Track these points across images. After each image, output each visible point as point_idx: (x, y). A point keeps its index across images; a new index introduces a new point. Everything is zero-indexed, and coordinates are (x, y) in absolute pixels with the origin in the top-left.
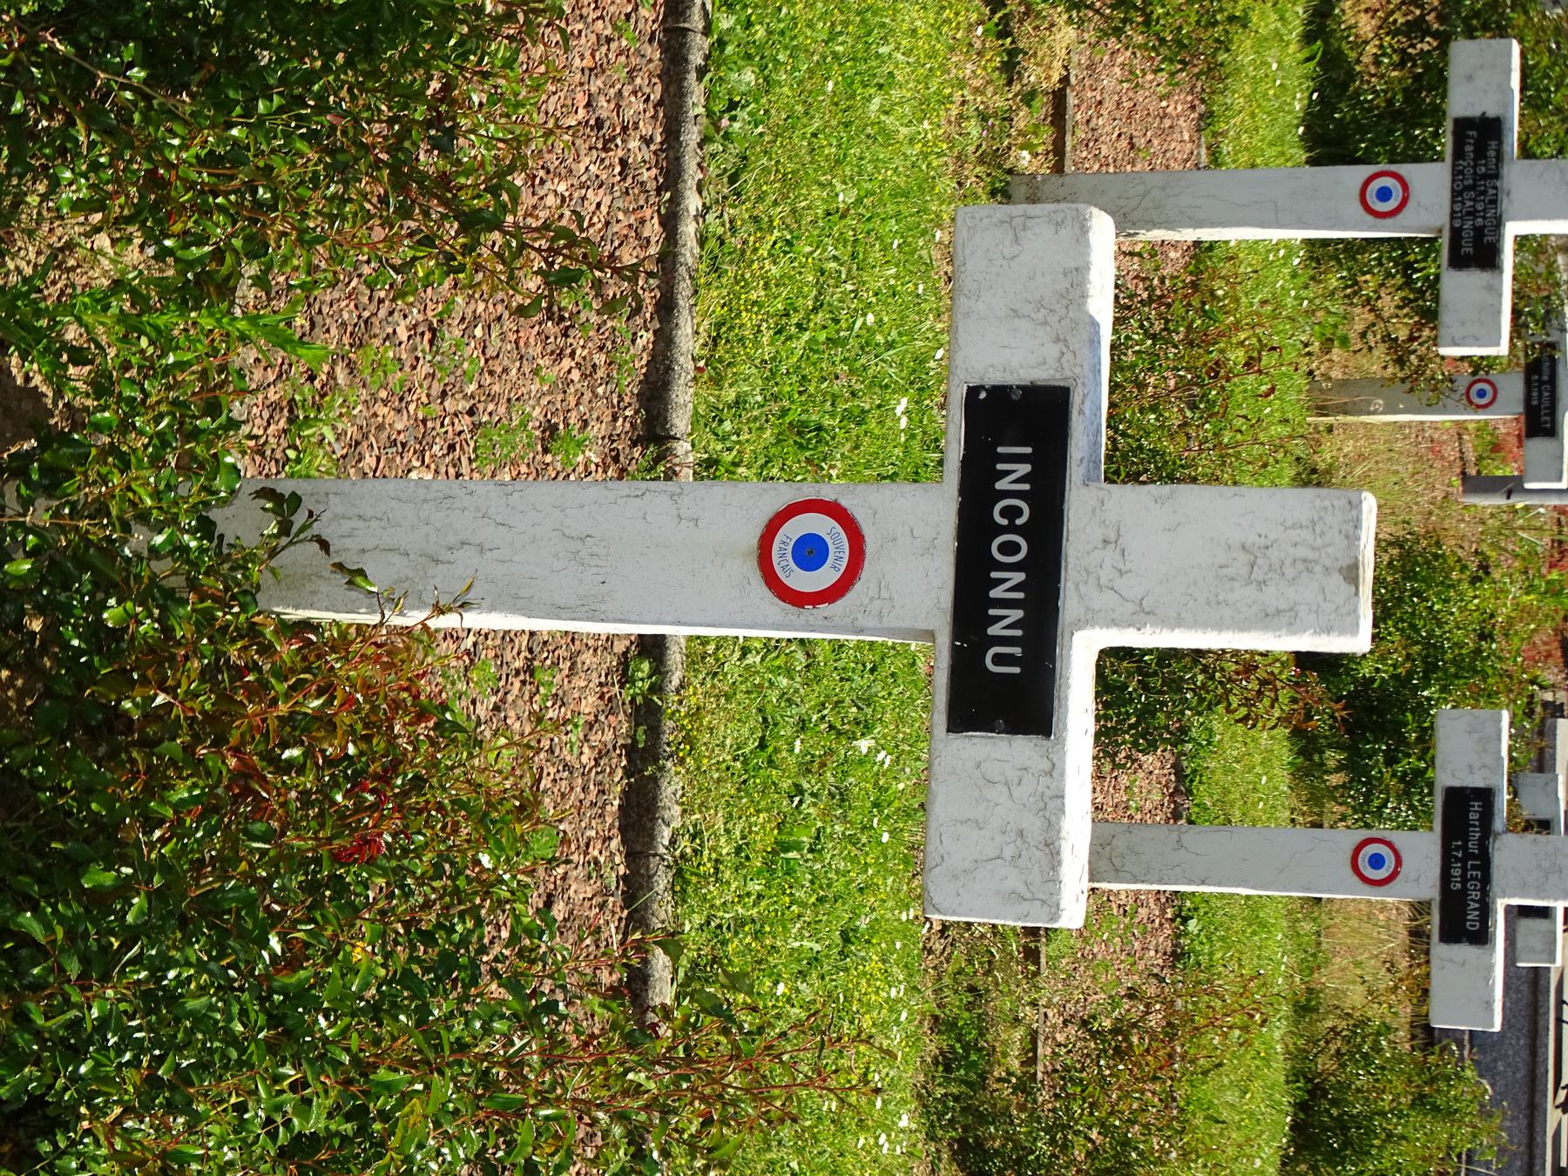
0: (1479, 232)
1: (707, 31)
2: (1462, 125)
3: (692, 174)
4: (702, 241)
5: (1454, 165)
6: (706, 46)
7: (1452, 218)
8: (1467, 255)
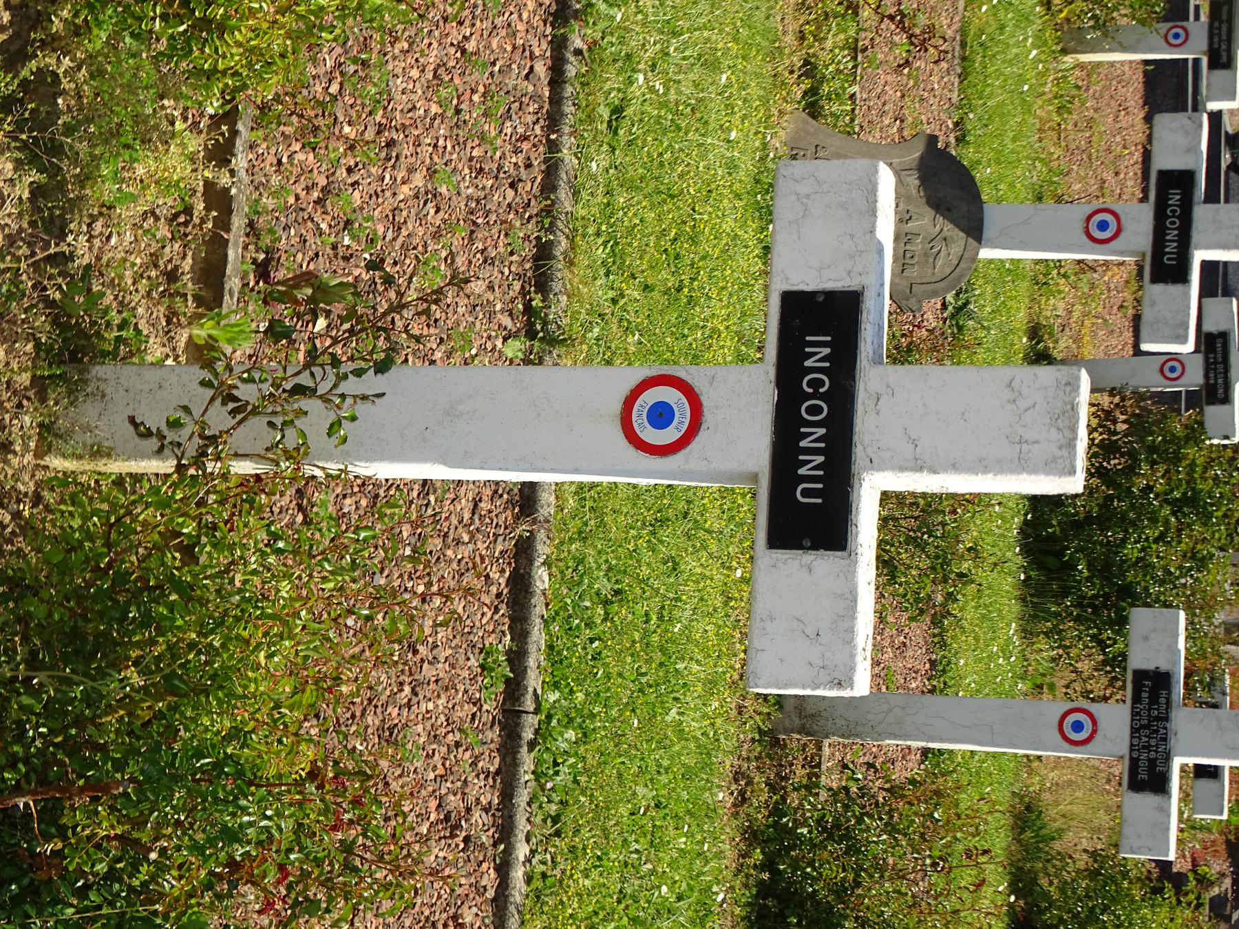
0: (1152, 763)
1: (537, 711)
2: (1140, 675)
3: (522, 826)
4: (529, 879)
5: (1133, 708)
6: (536, 723)
7: (1131, 750)
8: (1143, 780)
